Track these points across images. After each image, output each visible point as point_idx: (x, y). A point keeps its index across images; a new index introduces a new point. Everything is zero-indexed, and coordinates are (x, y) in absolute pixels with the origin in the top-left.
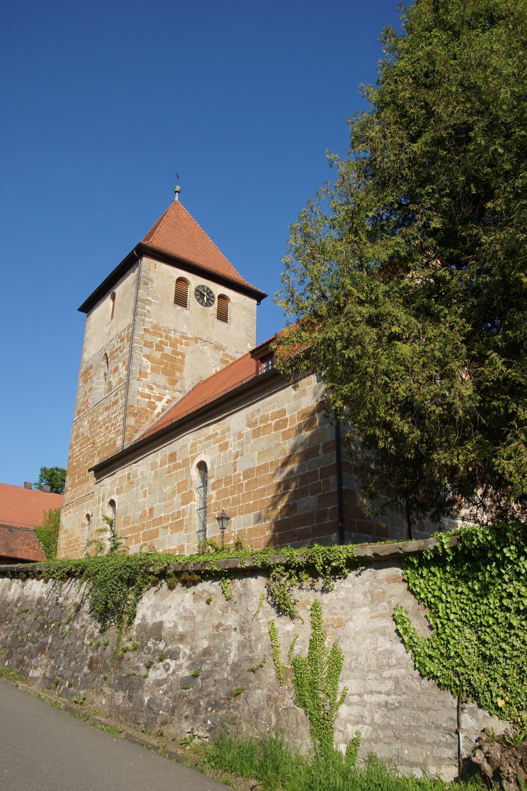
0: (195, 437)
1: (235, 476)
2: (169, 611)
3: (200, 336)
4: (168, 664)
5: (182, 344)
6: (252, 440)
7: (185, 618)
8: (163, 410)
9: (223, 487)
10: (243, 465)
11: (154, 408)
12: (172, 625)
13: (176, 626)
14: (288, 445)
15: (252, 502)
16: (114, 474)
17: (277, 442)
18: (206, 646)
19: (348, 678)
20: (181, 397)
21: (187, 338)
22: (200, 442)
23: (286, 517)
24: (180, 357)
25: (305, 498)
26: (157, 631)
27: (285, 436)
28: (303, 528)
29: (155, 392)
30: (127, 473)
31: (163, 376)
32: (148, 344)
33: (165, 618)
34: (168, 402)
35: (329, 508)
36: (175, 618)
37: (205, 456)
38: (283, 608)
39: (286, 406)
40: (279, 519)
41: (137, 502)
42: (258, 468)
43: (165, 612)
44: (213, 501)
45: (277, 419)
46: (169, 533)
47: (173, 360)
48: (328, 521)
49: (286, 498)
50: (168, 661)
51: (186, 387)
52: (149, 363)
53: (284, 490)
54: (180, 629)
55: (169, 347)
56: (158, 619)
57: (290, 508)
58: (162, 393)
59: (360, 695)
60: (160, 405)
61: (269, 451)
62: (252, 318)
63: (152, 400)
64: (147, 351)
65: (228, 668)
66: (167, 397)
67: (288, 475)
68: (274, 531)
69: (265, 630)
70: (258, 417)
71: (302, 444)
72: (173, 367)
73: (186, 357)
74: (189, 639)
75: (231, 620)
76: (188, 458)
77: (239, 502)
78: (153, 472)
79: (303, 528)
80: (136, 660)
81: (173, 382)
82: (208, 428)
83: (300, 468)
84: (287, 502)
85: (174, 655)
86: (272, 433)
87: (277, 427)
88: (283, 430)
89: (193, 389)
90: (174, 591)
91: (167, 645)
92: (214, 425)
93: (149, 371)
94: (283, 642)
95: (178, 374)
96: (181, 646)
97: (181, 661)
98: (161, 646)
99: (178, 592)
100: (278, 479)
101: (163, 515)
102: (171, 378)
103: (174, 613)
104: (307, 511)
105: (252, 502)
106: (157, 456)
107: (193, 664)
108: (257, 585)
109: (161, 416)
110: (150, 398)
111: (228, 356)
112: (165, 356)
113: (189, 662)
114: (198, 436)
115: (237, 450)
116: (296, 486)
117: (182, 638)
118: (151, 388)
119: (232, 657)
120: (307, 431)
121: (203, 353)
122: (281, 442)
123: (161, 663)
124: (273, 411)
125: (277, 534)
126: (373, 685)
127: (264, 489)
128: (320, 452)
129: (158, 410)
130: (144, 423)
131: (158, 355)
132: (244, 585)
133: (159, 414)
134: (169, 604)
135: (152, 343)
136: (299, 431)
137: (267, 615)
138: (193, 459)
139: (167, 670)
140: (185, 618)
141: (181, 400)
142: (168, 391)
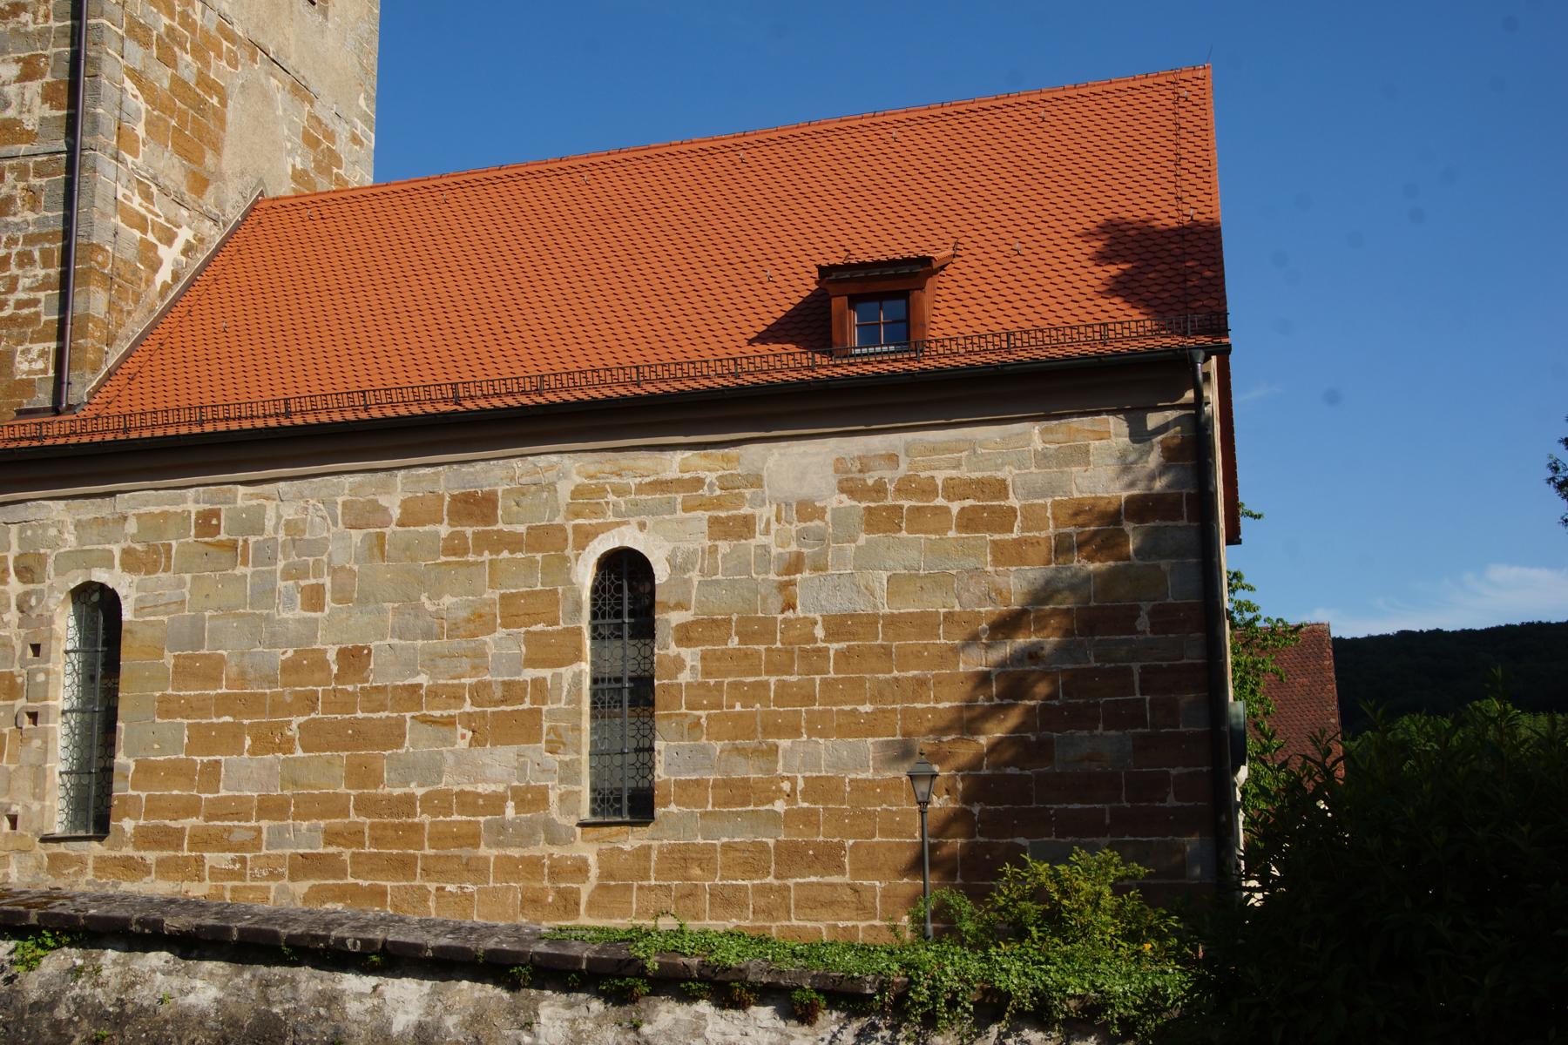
0: (592, 469)
3: (261, 41)
5: (219, 56)
6: (863, 538)
8: (176, 276)
9: (734, 642)
10: (817, 600)
11: (155, 266)
14: (1017, 583)
15: (868, 708)
16: (112, 494)
17: (971, 563)
20: (218, 239)
21: (231, 37)
22: (620, 491)
23: (1011, 770)
24: (215, 101)
25: (1085, 733)
27: (1002, 554)
28: (1077, 806)
29: (156, 210)
30: (194, 508)
31: (176, 160)
32: (138, 32)
34: (188, 250)
35: (1173, 772)
37: (641, 536)
39: (1007, 473)
40: (985, 771)
41: (267, 618)
42: (892, 621)
44: (684, 677)
45: (968, 503)
46: (462, 744)
47: (200, 106)
48: (1171, 801)
49: (1013, 719)
51: (228, 209)
52: (141, 104)
53: (1001, 696)
55: (188, 58)
57: (1020, 746)
58: (171, 215)
60: (170, 256)
61: (940, 581)
62: (370, 10)
63: (151, 237)
64: (136, 54)
66: (185, 235)
68: (968, 798)
70: (890, 476)
71: (1073, 588)
72: (200, 130)
73: (230, 103)
76: (562, 529)
77: (810, 699)
78: (357, 536)
79: (1077, 806)
81: (200, 183)
82: (657, 454)
83: (1062, 650)
84: (1016, 729)
86: (952, 534)
87: (969, 521)
88: (997, 537)
89: (245, 217)
92: (688, 454)
93: (140, 131)
95: (210, 159)
100: (977, 661)
101: (423, 679)
102: (194, 167)
105: (868, 708)
106: (397, 487)
109: (171, 295)
110: (144, 231)
111: (319, 122)
112: (178, 83)
114: (607, 468)
115: (794, 548)
116: (1050, 697)
118: (148, 196)
120: (1090, 559)
121: (266, 97)
124: (954, 473)
125: (976, 809)
127: (921, 682)
128: (1143, 623)
129: (164, 275)
130: (129, 313)
131: (162, 78)
133: (166, 287)
135: (147, 30)
136: (1063, 547)
138: (585, 536)
141: (223, 244)
142: (185, 213)
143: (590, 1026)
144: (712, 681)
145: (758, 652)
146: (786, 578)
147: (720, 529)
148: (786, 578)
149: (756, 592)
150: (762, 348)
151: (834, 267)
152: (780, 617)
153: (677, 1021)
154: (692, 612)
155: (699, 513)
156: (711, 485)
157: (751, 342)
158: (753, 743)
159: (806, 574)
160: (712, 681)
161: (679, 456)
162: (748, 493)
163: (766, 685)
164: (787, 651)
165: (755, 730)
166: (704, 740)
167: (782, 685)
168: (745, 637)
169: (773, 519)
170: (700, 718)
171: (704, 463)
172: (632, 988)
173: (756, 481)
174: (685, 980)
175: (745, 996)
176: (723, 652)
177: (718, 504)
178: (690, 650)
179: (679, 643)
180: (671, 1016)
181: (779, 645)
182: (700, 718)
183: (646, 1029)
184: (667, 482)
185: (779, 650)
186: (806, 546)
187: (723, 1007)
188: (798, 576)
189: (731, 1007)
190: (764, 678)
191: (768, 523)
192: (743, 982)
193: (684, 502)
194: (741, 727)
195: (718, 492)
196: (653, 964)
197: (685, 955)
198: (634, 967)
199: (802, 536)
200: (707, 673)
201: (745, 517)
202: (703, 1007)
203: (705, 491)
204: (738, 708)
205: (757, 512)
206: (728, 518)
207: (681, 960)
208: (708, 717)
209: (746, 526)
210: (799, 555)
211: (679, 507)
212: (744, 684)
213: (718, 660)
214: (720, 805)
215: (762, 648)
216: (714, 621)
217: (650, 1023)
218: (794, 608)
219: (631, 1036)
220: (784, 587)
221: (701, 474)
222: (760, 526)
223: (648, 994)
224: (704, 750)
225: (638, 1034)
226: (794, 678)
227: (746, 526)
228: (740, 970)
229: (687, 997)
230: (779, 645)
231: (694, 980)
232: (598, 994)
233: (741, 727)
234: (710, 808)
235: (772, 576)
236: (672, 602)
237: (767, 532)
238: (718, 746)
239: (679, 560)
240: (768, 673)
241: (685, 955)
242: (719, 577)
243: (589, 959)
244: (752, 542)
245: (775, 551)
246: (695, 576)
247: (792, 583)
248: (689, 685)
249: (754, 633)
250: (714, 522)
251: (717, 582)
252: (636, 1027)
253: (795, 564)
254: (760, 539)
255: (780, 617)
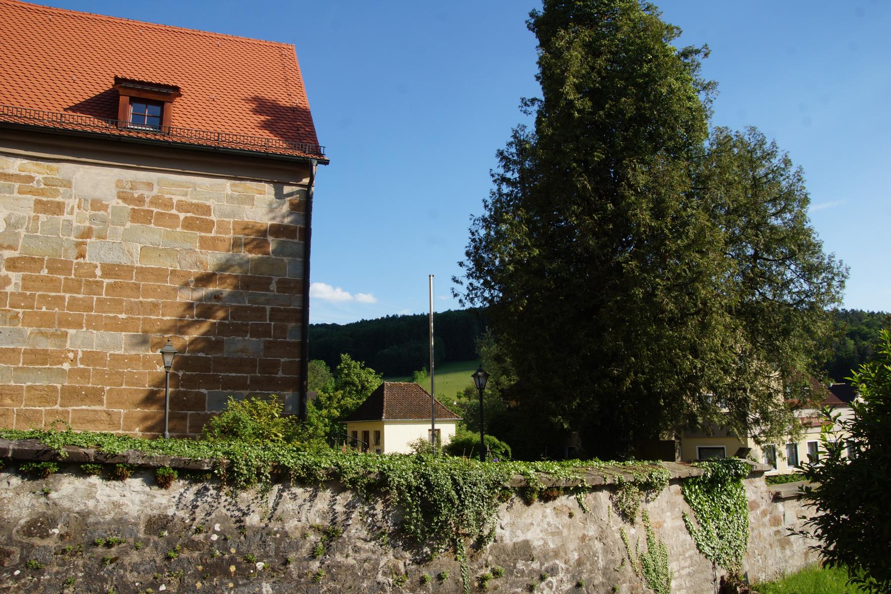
1: (78, 264)
2: (532, 529)
4: (550, 582)
7: (553, 534)
9: (45, 272)
12: (541, 543)
13: (546, 543)
15: (124, 316)
18: (576, 557)
19: (671, 562)
26: (525, 550)
28: (234, 374)
33: (529, 536)
36: (541, 535)
38: (627, 516)
42: (141, 271)
43: (528, 530)
44: (10, 289)
45: (189, 215)
49: (204, 328)
50: (549, 579)
53: (198, 316)
54: (552, 546)
56: (521, 537)
57: (209, 343)
59: (678, 571)
65: (600, 572)
67: (208, 297)
69: (618, 536)
71: (240, 265)
74: (562, 554)
75: (592, 531)
79: (234, 374)
80: (508, 586)
84: (205, 334)
85: (553, 571)
88: (203, 234)
90: (532, 507)
91: (542, 564)
94: (631, 543)
96: (557, 562)
97: (561, 575)
98: (535, 565)
99: (536, 508)
103: (538, 530)
104: (244, 356)
105: (124, 316)
107: (573, 576)
108: (604, 495)
113: (569, 576)
115: (87, 224)
116: (224, 319)
117: (556, 554)
119: (601, 564)
122: (197, 250)
123: (543, 583)
124: (183, 198)
126: (683, 564)
132: (595, 498)
134: (529, 521)
136: (236, 244)
137: (616, 523)
139: (551, 588)
140: (553, 534)
143: (10, 494)
144: (28, 293)
145: (59, 279)
146: (81, 240)
147: (41, 207)
148: (81, 240)
149: (62, 246)
150: (71, 113)
151: (125, 80)
152: (75, 261)
153: (76, 489)
154: (18, 252)
155: (29, 196)
156: (38, 182)
157: (65, 110)
158: (52, 330)
159: (93, 239)
160: (28, 293)
161: (19, 162)
162: (62, 190)
163: (63, 298)
164: (77, 281)
165: (54, 323)
166: (20, 326)
167: (73, 299)
168: (51, 270)
169: (76, 206)
170: (18, 313)
171: (35, 168)
172: (45, 469)
173: (68, 184)
174: (84, 463)
175: (125, 472)
176: (37, 277)
177: (42, 193)
178: (14, 274)
179: (8, 268)
180: (71, 486)
181: (73, 276)
182: (18, 313)
183: (53, 495)
184: (9, 175)
185: (73, 279)
186: (94, 224)
187: (108, 479)
188: (88, 240)
189: (114, 479)
190: (62, 294)
191: (73, 208)
192: (125, 463)
193: (19, 188)
194: (46, 320)
195: (43, 186)
196: (63, 452)
197: (83, 447)
198: (50, 455)
199: (93, 218)
200: (25, 288)
201: (59, 203)
202: (95, 479)
203: (34, 184)
204: (44, 309)
205: (67, 201)
206: (48, 202)
207: (82, 450)
208: (24, 313)
209: (59, 208)
210: (90, 229)
211: (16, 190)
212: (49, 296)
213: (34, 281)
214: (27, 364)
215: (62, 277)
216: (33, 259)
217: (56, 491)
218: (84, 257)
219: (43, 500)
220: (78, 245)
221: (33, 175)
222: (67, 209)
223: (56, 472)
224: (20, 332)
225: (48, 498)
226: (81, 296)
227: (59, 208)
228: (124, 456)
229: (84, 473)
230: (73, 276)
231: (90, 463)
232: (17, 473)
233: (46, 320)
234: (20, 365)
235: (72, 238)
236: (5, 245)
237: (71, 213)
238: (29, 330)
239: (12, 221)
240: (64, 291)
241: (83, 447)
242: (39, 234)
243: (14, 450)
244: (62, 218)
245: (75, 224)
246: (23, 232)
247: (85, 243)
248: (12, 294)
249: (58, 268)
250: (38, 202)
251: (37, 237)
252: (46, 494)
253: (87, 233)
254: (66, 216)
255: (75, 261)
